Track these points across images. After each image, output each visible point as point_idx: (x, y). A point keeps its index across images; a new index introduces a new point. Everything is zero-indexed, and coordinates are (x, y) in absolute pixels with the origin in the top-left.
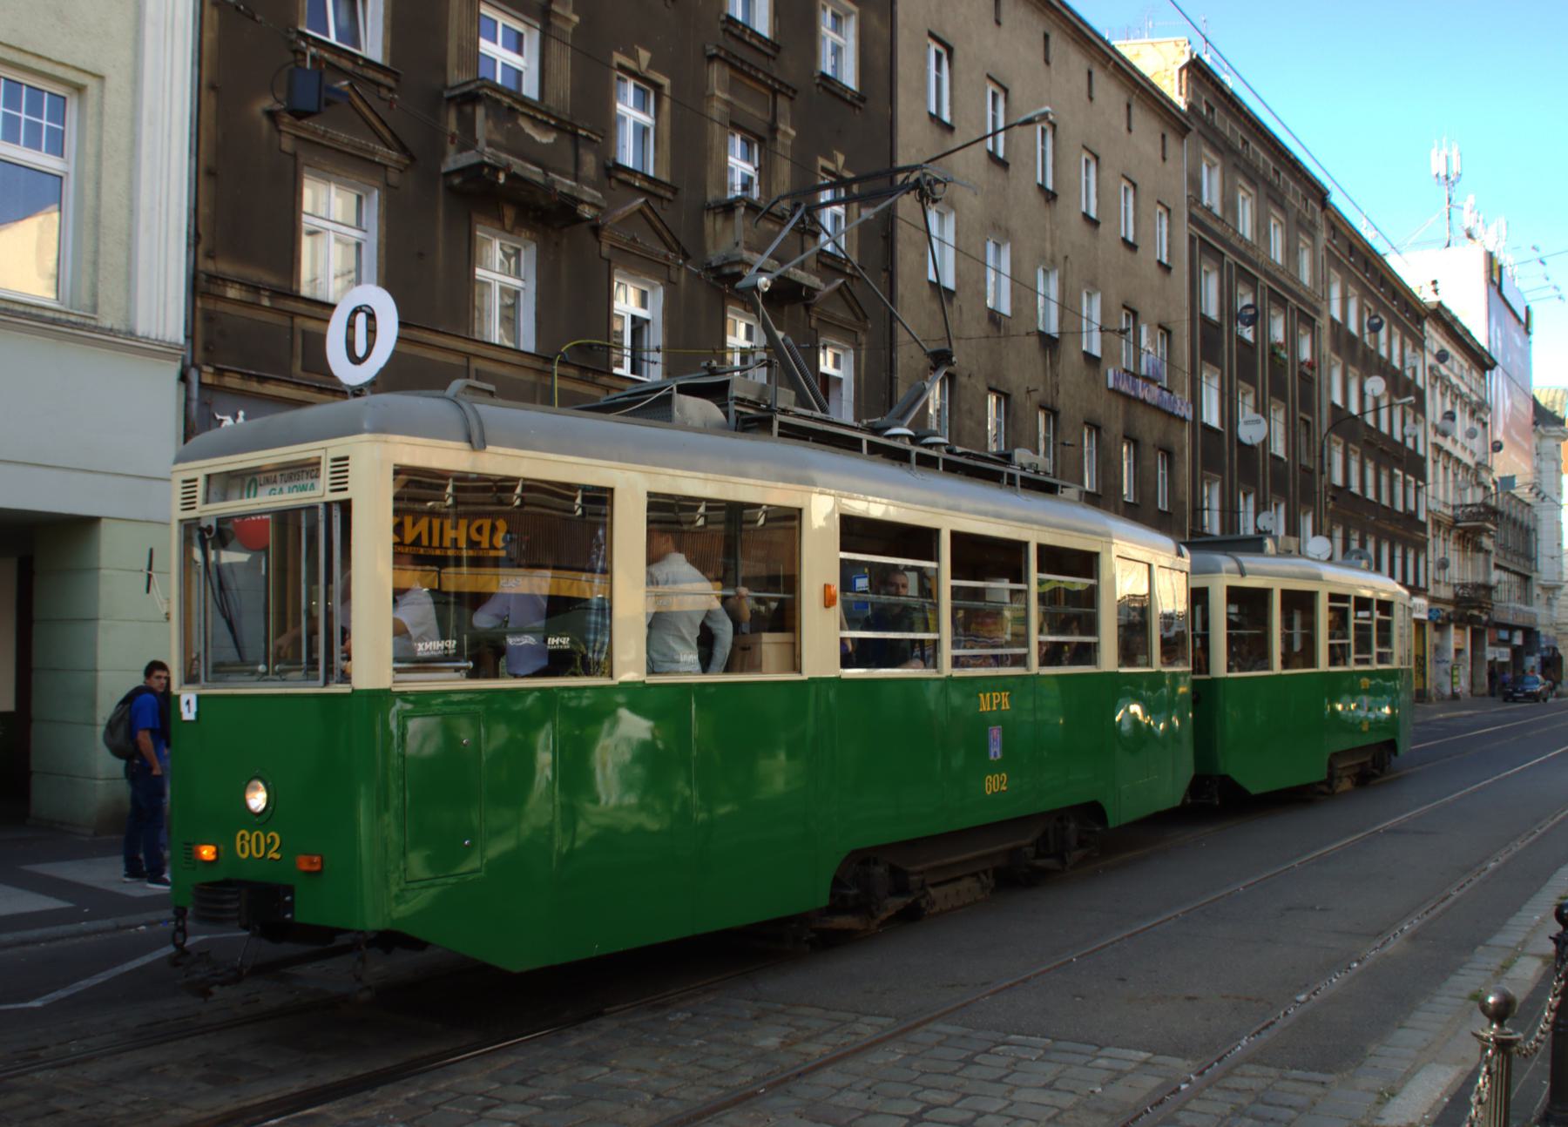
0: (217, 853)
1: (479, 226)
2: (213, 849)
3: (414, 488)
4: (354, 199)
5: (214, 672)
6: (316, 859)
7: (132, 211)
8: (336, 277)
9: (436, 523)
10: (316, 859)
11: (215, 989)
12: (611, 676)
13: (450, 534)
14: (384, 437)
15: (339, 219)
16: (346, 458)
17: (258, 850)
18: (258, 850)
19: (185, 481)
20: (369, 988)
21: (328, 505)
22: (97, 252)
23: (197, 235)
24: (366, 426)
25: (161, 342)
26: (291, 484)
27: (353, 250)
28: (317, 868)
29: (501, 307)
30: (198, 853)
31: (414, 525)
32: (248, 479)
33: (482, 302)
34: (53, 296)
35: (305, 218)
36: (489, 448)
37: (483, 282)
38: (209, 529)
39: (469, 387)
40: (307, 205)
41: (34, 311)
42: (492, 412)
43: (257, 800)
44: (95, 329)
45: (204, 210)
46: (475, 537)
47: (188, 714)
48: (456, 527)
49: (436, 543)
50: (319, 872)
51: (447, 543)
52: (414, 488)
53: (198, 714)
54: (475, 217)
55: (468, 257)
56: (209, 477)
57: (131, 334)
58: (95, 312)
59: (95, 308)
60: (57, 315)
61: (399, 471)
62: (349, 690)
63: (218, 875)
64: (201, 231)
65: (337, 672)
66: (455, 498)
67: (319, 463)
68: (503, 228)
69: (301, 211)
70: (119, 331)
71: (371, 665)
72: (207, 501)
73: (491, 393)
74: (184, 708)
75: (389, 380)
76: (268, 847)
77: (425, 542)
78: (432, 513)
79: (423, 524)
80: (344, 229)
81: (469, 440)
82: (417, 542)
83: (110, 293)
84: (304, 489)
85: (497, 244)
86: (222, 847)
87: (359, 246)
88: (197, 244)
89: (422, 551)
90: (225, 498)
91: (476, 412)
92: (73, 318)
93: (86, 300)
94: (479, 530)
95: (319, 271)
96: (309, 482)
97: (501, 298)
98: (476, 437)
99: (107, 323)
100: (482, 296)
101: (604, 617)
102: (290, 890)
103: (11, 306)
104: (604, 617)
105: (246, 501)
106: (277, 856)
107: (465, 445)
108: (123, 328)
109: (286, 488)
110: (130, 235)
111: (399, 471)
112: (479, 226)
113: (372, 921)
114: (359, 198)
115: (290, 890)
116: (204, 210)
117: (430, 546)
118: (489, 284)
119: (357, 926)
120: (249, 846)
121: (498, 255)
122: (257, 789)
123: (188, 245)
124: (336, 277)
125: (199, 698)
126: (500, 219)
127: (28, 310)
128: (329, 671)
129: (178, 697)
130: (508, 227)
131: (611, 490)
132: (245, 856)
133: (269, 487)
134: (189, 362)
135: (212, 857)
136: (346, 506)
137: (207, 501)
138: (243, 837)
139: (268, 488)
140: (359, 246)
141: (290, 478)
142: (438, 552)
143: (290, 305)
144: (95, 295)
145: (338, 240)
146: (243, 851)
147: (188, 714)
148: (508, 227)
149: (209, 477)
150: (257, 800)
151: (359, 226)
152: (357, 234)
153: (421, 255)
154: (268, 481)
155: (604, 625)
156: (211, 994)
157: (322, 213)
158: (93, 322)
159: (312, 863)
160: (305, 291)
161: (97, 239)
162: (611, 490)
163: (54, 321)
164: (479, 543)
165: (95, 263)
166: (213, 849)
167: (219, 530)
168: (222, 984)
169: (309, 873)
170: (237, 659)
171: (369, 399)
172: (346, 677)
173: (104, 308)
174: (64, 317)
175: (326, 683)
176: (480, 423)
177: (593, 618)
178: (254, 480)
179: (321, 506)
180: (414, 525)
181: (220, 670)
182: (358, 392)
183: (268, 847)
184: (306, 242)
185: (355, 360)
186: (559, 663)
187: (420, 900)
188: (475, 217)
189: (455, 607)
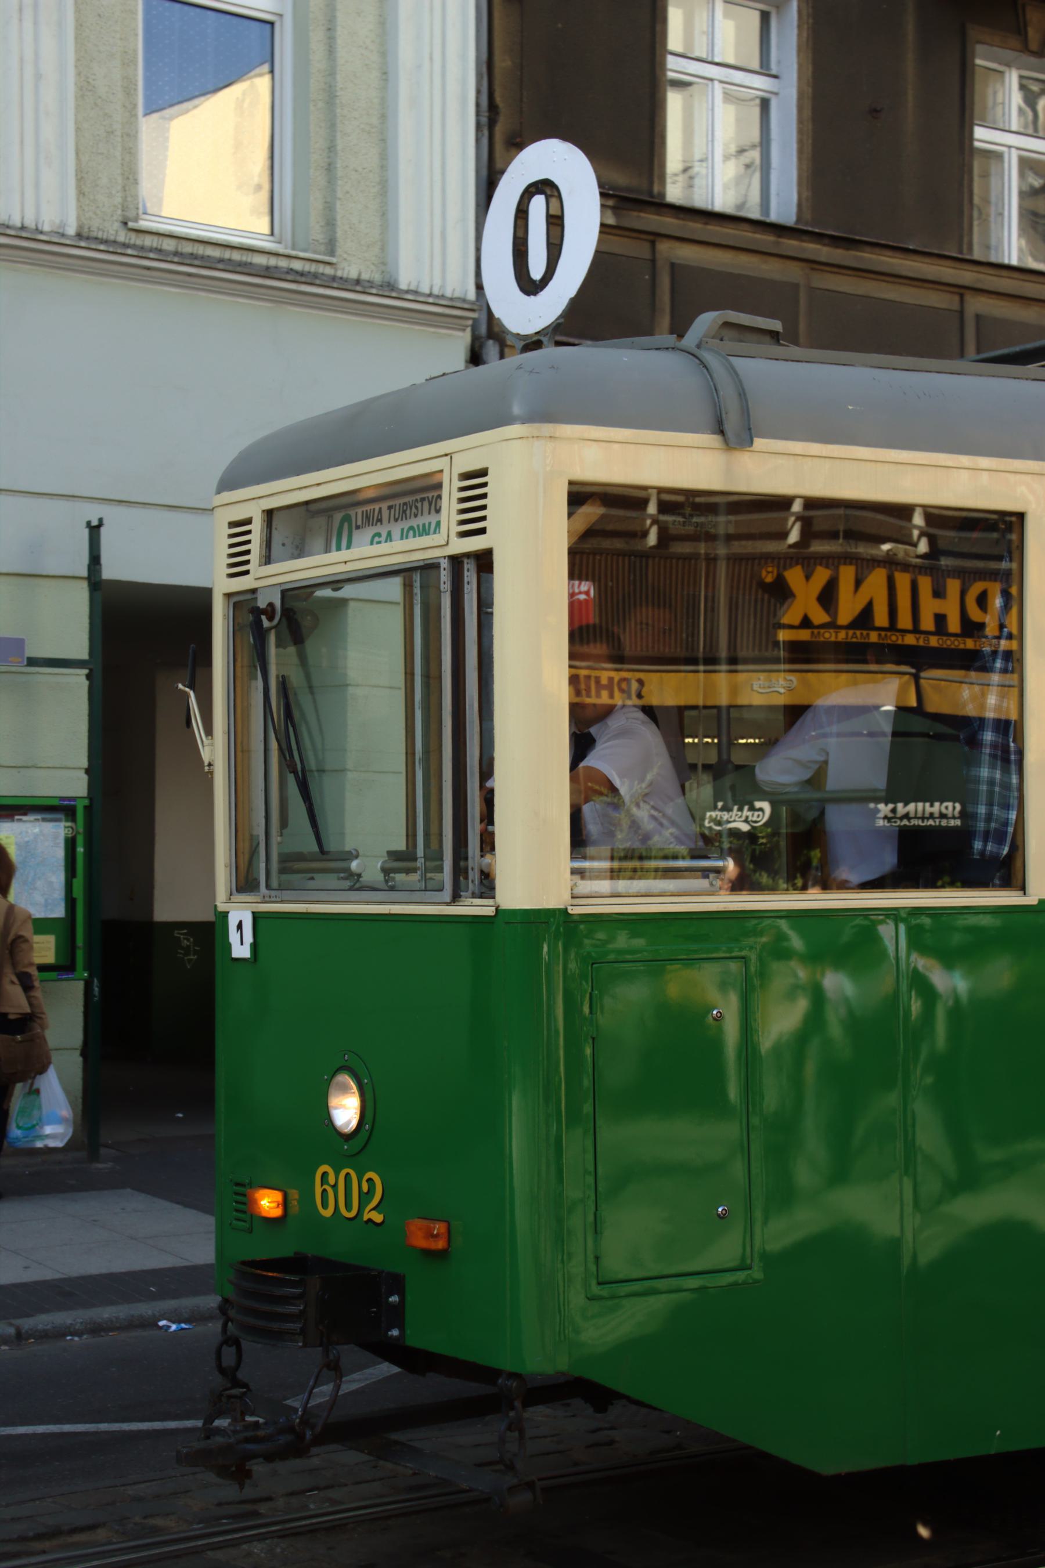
0: (285, 1203)
1: (979, 48)
2: (278, 1196)
3: (609, 530)
4: (755, 18)
5: (282, 871)
6: (438, 1228)
7: (386, 75)
8: (727, 158)
9: (903, 581)
10: (438, 1228)
11: (258, 1468)
12: (1023, 888)
13: (929, 607)
14: (547, 428)
15: (731, 61)
16: (484, 473)
17: (348, 1206)
18: (348, 1206)
19: (233, 524)
20: (530, 1486)
21: (456, 561)
22: (331, 149)
23: (492, 107)
24: (516, 410)
25: (438, 299)
26: (405, 525)
27: (756, 111)
28: (440, 1244)
29: (1022, 194)
30: (254, 1203)
31: (858, 583)
32: (338, 516)
33: (987, 190)
34: (262, 225)
35: (672, 62)
36: (759, 443)
37: (987, 154)
38: (270, 611)
39: (727, 325)
40: (675, 41)
41: (236, 256)
42: (765, 372)
43: (346, 1110)
44: (333, 282)
45: (503, 63)
46: (975, 614)
47: (241, 950)
48: (939, 593)
49: (905, 620)
50: (442, 1255)
51: (927, 623)
52: (609, 530)
53: (254, 947)
54: (973, 32)
55: (961, 108)
56: (269, 514)
57: (389, 287)
58: (332, 253)
59: (331, 246)
60: (273, 261)
61: (578, 496)
62: (490, 911)
63: (283, 1248)
64: (498, 99)
65: (474, 875)
66: (932, 541)
67: (439, 486)
68: (1026, 49)
69: (665, 51)
70: (371, 283)
71: (532, 866)
72: (267, 559)
73: (774, 335)
74: (234, 937)
75: (579, 323)
76: (365, 1197)
77: (881, 618)
78: (890, 562)
79: (876, 582)
80: (739, 77)
81: (720, 430)
82: (864, 619)
83: (355, 214)
84: (424, 531)
85: (1013, 78)
86: (294, 1194)
87: (765, 104)
88: (492, 123)
89: (874, 637)
90: (300, 552)
91: (734, 372)
92: (297, 265)
93: (317, 233)
94: (982, 601)
95: (699, 150)
96: (432, 519)
97: (1022, 175)
98: (732, 423)
99: (351, 271)
100: (986, 175)
101: (1006, 771)
102: (397, 1283)
103: (200, 250)
104: (1006, 771)
105: (334, 556)
106: (378, 1218)
107: (712, 440)
108: (377, 278)
109: (396, 529)
110: (383, 117)
111: (578, 496)
112: (979, 48)
113: (537, 1357)
114: (765, 17)
115: (397, 1283)
116: (503, 63)
117: (893, 626)
118: (999, 156)
119: (505, 1363)
120: (342, 1196)
121: (1016, 98)
122: (345, 1089)
123: (479, 126)
124: (727, 158)
125: (256, 917)
126: (1019, 30)
127: (227, 254)
128: (460, 871)
129: (225, 915)
130: (1034, 45)
131: (1021, 516)
132: (328, 1213)
133: (370, 531)
134: (483, 330)
135: (277, 1212)
136: (484, 561)
137: (267, 559)
138: (325, 1175)
139: (369, 532)
140: (765, 104)
141: (403, 514)
142: (910, 640)
143: (651, 220)
144: (330, 223)
145: (728, 97)
146: (325, 1205)
147: (241, 950)
148: (1034, 45)
149: (269, 514)
150: (346, 1110)
151: (765, 69)
152: (760, 82)
153: (875, 112)
154: (371, 520)
155: (1006, 786)
156: (248, 1474)
157: (701, 52)
158: (328, 271)
159: (430, 1235)
160: (674, 193)
161: (332, 126)
162: (1021, 516)
163: (267, 272)
164: (981, 626)
165: (330, 168)
166: (278, 1196)
167: (288, 613)
168: (269, 1458)
169: (429, 1254)
170: (316, 849)
171: (549, 353)
172: (487, 885)
173: (345, 245)
174: (283, 263)
175: (456, 897)
176: (742, 395)
177: (985, 772)
178: (347, 519)
179: (444, 564)
180: (858, 583)
181: (294, 869)
182: (533, 344)
183: (365, 1197)
184: (674, 102)
185: (530, 287)
186: (924, 858)
187: (630, 1319)
188: (973, 32)
189: (712, 753)
